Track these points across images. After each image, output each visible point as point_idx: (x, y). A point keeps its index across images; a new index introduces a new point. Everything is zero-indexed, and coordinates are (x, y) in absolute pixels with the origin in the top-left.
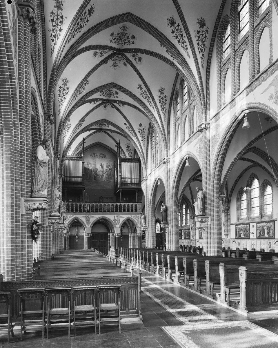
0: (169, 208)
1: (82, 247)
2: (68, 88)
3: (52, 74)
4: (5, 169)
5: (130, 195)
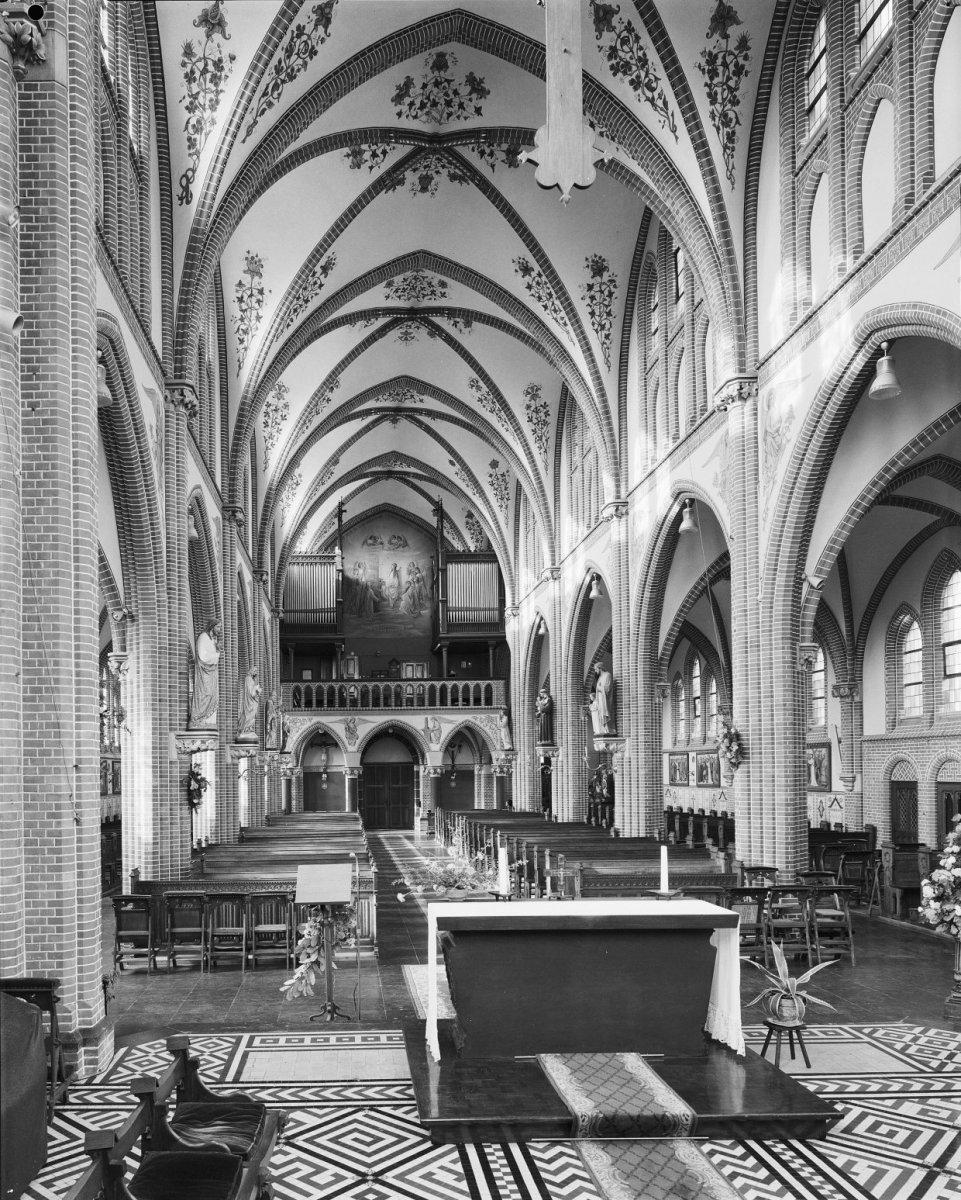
0: (558, 703)
1: (341, 808)
2: (286, 406)
3: (240, 415)
4: (142, 684)
5: (473, 654)
